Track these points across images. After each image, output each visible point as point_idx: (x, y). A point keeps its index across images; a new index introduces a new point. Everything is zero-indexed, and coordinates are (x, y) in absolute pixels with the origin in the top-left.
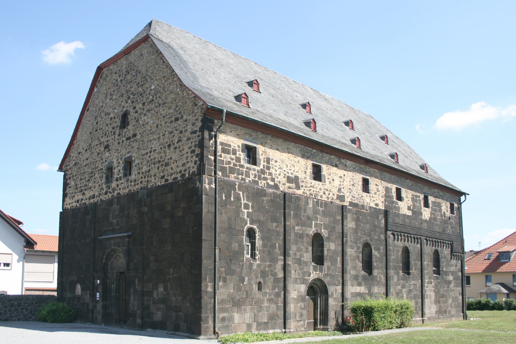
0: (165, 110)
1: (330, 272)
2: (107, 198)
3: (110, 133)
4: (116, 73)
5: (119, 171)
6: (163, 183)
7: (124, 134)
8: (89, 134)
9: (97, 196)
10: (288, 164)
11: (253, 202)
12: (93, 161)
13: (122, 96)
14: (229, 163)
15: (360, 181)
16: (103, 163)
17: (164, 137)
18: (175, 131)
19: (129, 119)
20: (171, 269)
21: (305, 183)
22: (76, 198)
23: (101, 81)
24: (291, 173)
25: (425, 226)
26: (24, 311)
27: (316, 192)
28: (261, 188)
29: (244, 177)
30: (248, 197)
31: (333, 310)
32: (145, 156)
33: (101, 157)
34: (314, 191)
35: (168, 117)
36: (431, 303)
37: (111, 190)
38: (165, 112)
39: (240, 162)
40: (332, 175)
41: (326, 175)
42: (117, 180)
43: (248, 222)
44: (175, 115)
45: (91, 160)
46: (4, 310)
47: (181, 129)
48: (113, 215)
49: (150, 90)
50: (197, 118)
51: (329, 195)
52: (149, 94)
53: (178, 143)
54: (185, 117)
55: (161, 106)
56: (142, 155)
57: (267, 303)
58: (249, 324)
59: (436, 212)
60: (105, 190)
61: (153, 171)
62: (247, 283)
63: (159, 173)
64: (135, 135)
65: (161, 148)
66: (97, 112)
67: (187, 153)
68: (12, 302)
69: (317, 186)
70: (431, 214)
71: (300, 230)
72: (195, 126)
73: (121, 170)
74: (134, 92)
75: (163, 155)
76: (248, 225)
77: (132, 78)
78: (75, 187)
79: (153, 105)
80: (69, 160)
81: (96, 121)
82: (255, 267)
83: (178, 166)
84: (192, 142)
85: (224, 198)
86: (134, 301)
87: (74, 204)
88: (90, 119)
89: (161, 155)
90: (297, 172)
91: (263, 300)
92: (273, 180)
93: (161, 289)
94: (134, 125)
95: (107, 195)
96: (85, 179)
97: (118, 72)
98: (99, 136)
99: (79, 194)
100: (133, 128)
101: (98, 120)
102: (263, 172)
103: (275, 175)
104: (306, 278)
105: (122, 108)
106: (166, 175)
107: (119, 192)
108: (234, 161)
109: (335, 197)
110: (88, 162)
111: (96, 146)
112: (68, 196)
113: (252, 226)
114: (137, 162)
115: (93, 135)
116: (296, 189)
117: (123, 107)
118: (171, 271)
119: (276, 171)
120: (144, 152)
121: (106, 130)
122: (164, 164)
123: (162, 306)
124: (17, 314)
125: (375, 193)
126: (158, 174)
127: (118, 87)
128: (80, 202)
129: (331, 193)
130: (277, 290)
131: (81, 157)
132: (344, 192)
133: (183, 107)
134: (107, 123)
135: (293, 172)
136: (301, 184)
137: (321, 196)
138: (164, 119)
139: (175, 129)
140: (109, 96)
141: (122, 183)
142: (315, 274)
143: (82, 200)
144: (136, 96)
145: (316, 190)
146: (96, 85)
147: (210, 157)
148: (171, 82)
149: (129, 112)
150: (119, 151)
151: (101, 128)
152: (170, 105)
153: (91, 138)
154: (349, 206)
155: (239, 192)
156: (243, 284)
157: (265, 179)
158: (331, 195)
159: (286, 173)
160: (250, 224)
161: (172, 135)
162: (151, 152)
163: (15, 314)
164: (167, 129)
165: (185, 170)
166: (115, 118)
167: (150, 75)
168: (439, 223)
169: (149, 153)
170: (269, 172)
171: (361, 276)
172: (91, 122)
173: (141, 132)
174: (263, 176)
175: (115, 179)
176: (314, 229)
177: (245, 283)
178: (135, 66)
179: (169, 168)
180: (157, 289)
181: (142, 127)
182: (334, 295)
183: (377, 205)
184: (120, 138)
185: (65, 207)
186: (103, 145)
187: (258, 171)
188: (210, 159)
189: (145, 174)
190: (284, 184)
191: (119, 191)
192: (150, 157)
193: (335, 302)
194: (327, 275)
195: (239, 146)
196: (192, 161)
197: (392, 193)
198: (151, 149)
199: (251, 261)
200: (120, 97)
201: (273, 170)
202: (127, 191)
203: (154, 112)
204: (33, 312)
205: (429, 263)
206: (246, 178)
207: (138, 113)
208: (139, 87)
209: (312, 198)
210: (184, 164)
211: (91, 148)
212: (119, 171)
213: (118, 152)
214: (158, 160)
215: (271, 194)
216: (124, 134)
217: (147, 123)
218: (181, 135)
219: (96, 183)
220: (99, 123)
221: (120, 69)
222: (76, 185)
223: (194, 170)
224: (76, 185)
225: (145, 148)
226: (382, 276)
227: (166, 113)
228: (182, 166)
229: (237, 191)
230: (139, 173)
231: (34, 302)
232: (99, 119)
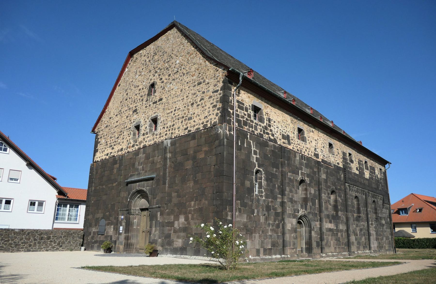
0: (189, 77)
1: (312, 211)
2: (134, 149)
3: (138, 100)
4: (145, 56)
5: (146, 128)
6: (186, 133)
7: (151, 100)
8: (120, 103)
9: (124, 149)
10: (283, 125)
11: (260, 150)
12: (122, 122)
13: (150, 71)
14: (243, 117)
15: (328, 145)
16: (132, 123)
17: (188, 98)
18: (198, 93)
19: (156, 88)
20: (193, 202)
21: (294, 141)
22: (106, 152)
23: (132, 64)
24: (285, 132)
25: (366, 182)
26: (53, 243)
27: (301, 148)
28: (265, 140)
29: (253, 130)
30: (256, 145)
31: (315, 241)
32: (170, 114)
33: (130, 119)
34: (299, 148)
35: (191, 82)
36: (374, 240)
37: (137, 143)
38: (189, 79)
39: (251, 118)
40: (310, 137)
41: (307, 137)
42: (144, 135)
43: (257, 166)
44: (197, 81)
45: (121, 122)
46: (34, 242)
47: (203, 90)
48: (139, 163)
49: (176, 64)
50: (218, 80)
51: (309, 152)
52: (175, 67)
53: (200, 101)
54: (207, 80)
55: (185, 75)
56: (167, 114)
57: (270, 232)
58: (258, 249)
59: (372, 174)
60: (132, 143)
61: (177, 125)
62: (256, 215)
63: (183, 126)
64: (161, 100)
65: (185, 107)
66: (128, 86)
67: (209, 108)
68: (42, 236)
69: (302, 144)
70: (370, 175)
71: (291, 176)
72: (216, 87)
73: (148, 127)
74: (161, 68)
75: (186, 111)
76: (257, 167)
77: (159, 58)
78: (105, 144)
79: (178, 75)
80: (101, 124)
81: (127, 93)
82: (261, 202)
83: (200, 119)
84: (213, 100)
85: (240, 144)
86: (155, 231)
87: (104, 157)
88: (121, 92)
89: (184, 112)
90: (289, 132)
91: (268, 229)
92: (273, 135)
93: (182, 219)
94: (160, 92)
95: (134, 148)
96: (115, 137)
97: (146, 55)
98: (128, 103)
99: (108, 148)
100: (159, 94)
101: (128, 92)
102: (266, 128)
103: (274, 131)
104: (296, 214)
105: (149, 81)
106: (189, 127)
107: (145, 144)
108: (247, 116)
109: (313, 154)
110: (118, 123)
111: (125, 111)
112: (99, 151)
113: (259, 169)
114: (162, 120)
115: (123, 104)
116: (288, 144)
117: (151, 80)
118: (193, 203)
119: (275, 129)
120: (169, 111)
121: (135, 98)
122: (187, 119)
123: (182, 234)
124: (45, 246)
125: (337, 155)
126: (181, 127)
127: (147, 65)
128: (109, 155)
129: (310, 151)
130: (277, 222)
131: (112, 121)
132: (318, 151)
133: (205, 74)
134: (136, 93)
135: (286, 131)
136: (291, 141)
137: (304, 152)
138: (187, 84)
139: (198, 91)
140: (138, 73)
141: (148, 137)
142: (302, 211)
143: (111, 153)
144: (162, 71)
145: (301, 148)
146: (127, 67)
147: (229, 110)
148: (195, 56)
149: (156, 83)
150: (146, 113)
151: (130, 97)
152: (193, 73)
153: (121, 106)
154: (322, 162)
155: (250, 141)
156: (253, 215)
157: (268, 134)
158: (310, 153)
159: (281, 131)
160: (258, 167)
161: (195, 95)
162: (175, 110)
163: (44, 246)
164: (190, 92)
165: (207, 122)
166: (143, 89)
167: (175, 53)
168: (374, 181)
169: (173, 112)
170: (270, 129)
171: (331, 216)
172: (122, 94)
173: (167, 96)
174: (266, 131)
175: (142, 134)
176: (300, 176)
177: (255, 215)
178: (162, 48)
179: (192, 121)
180: (178, 220)
181: (167, 93)
182: (315, 229)
183: (338, 164)
184: (148, 103)
185: (96, 160)
186: (132, 110)
187: (263, 127)
188: (230, 111)
189: (170, 128)
190: (280, 140)
191: (145, 143)
192: (174, 114)
193: (316, 235)
194: (310, 212)
195: (249, 106)
196: (213, 114)
197: (346, 157)
198: (175, 109)
199: (259, 197)
200: (148, 73)
201: (273, 128)
202: (152, 142)
203: (178, 80)
204: (61, 245)
205: (371, 210)
206: (255, 131)
207: (164, 83)
208: (165, 63)
209: (299, 153)
210: (206, 117)
211: (121, 113)
212: (146, 128)
213: (145, 113)
214: (182, 116)
215: (272, 145)
216: (151, 100)
217: (173, 89)
218: (204, 95)
219: (124, 139)
220: (129, 94)
221: (149, 52)
222: (107, 142)
223: (215, 120)
224: (107, 142)
225: (170, 108)
226: (344, 216)
227: (190, 79)
228: (204, 119)
229: (249, 140)
230: (164, 128)
231: (63, 236)
232: (129, 91)
